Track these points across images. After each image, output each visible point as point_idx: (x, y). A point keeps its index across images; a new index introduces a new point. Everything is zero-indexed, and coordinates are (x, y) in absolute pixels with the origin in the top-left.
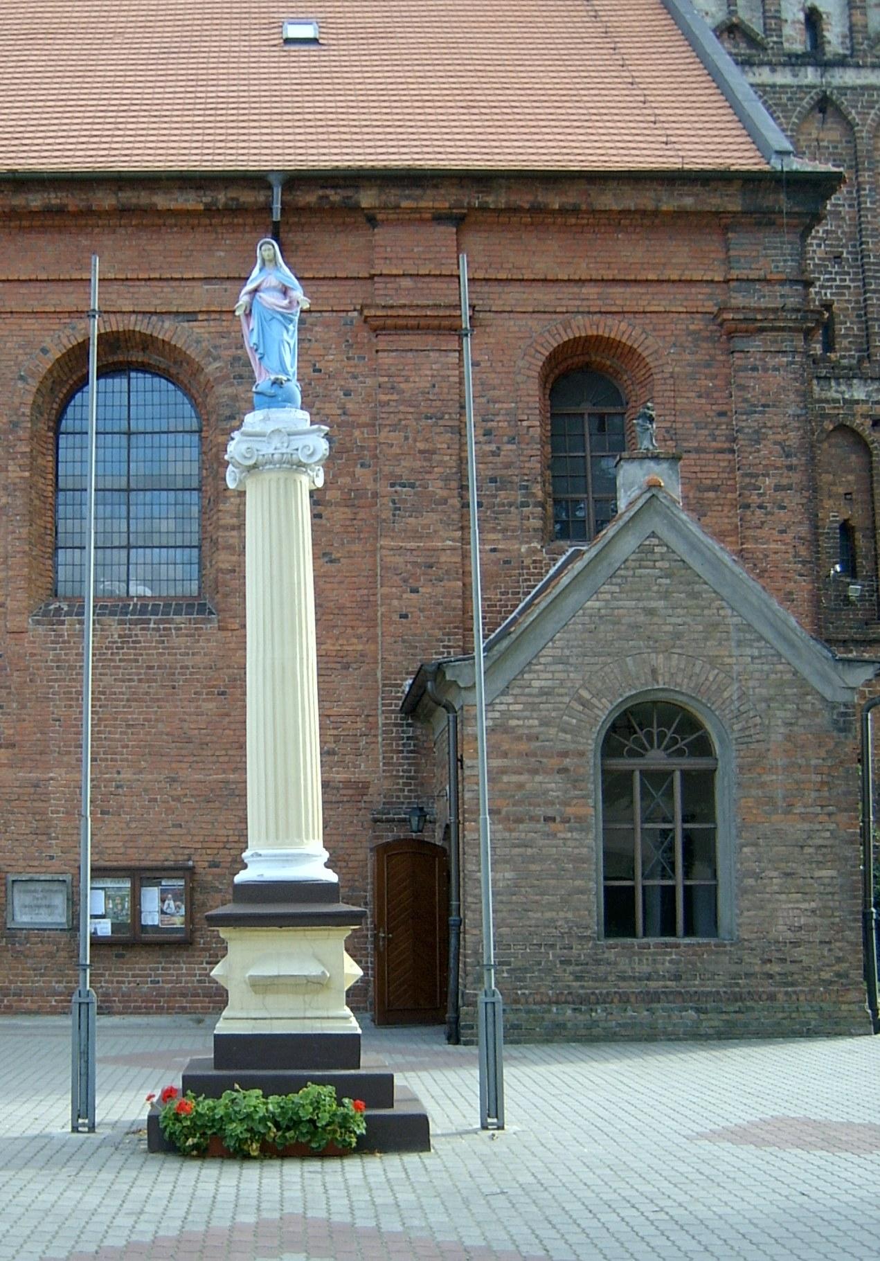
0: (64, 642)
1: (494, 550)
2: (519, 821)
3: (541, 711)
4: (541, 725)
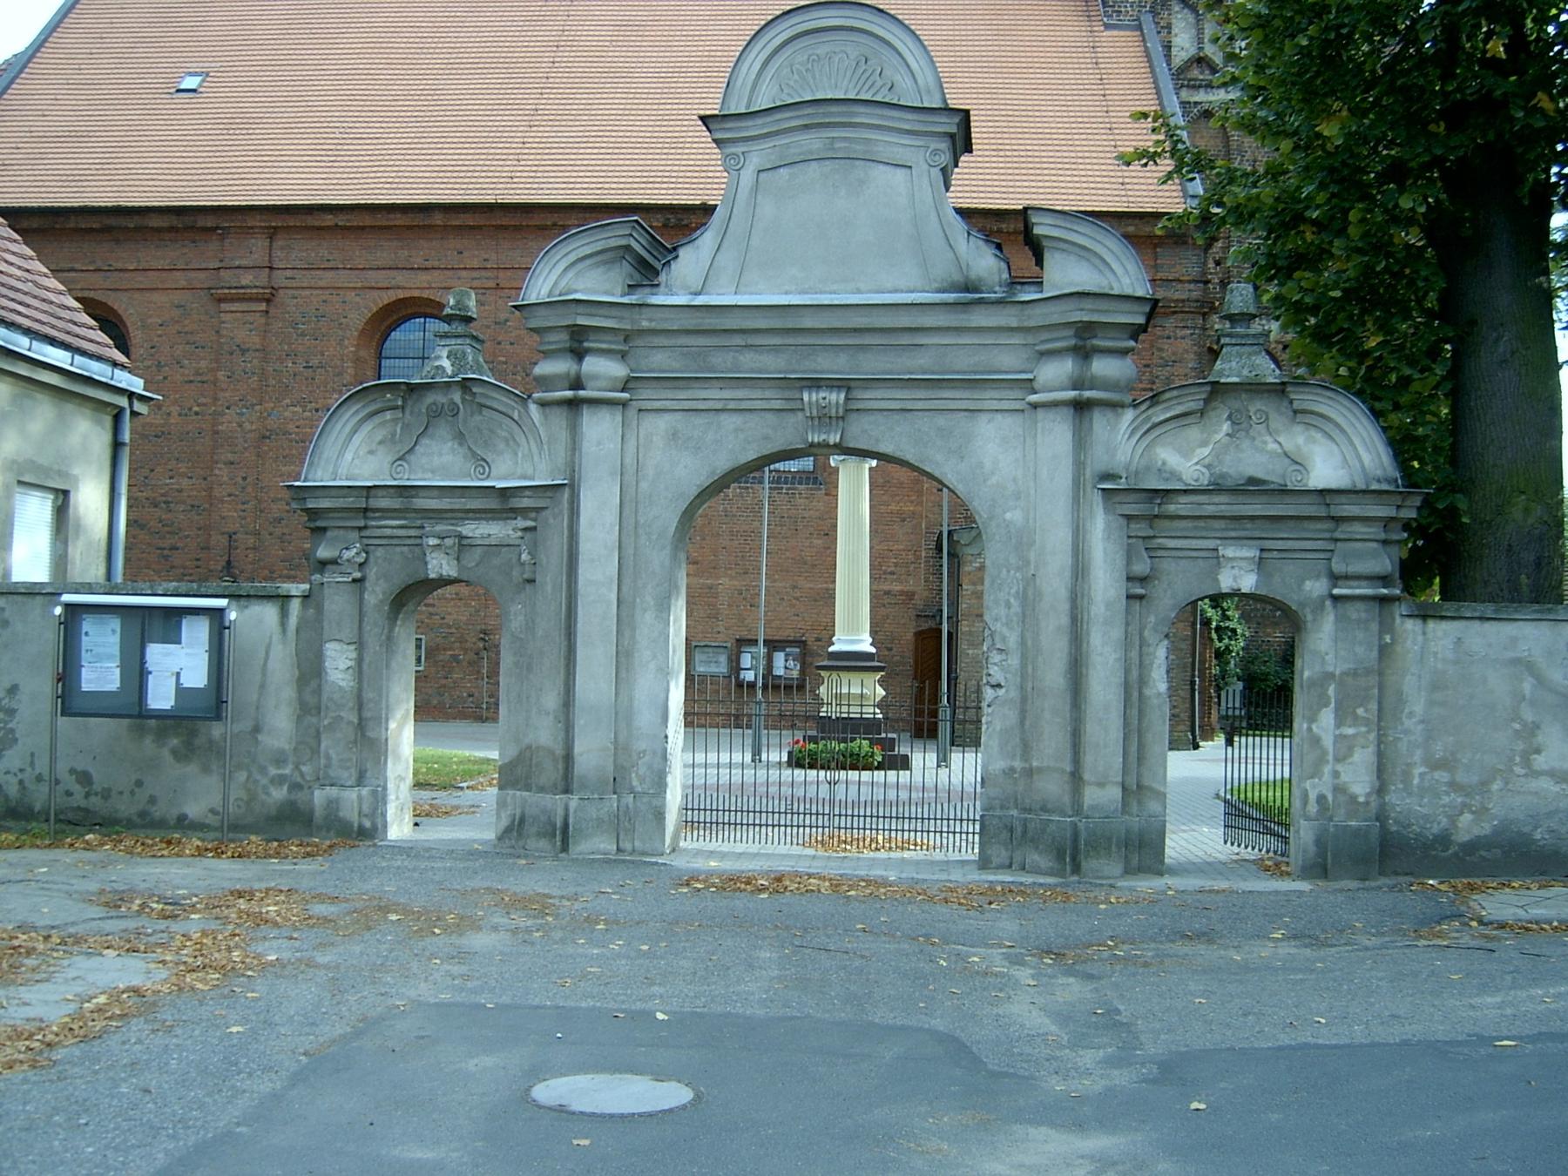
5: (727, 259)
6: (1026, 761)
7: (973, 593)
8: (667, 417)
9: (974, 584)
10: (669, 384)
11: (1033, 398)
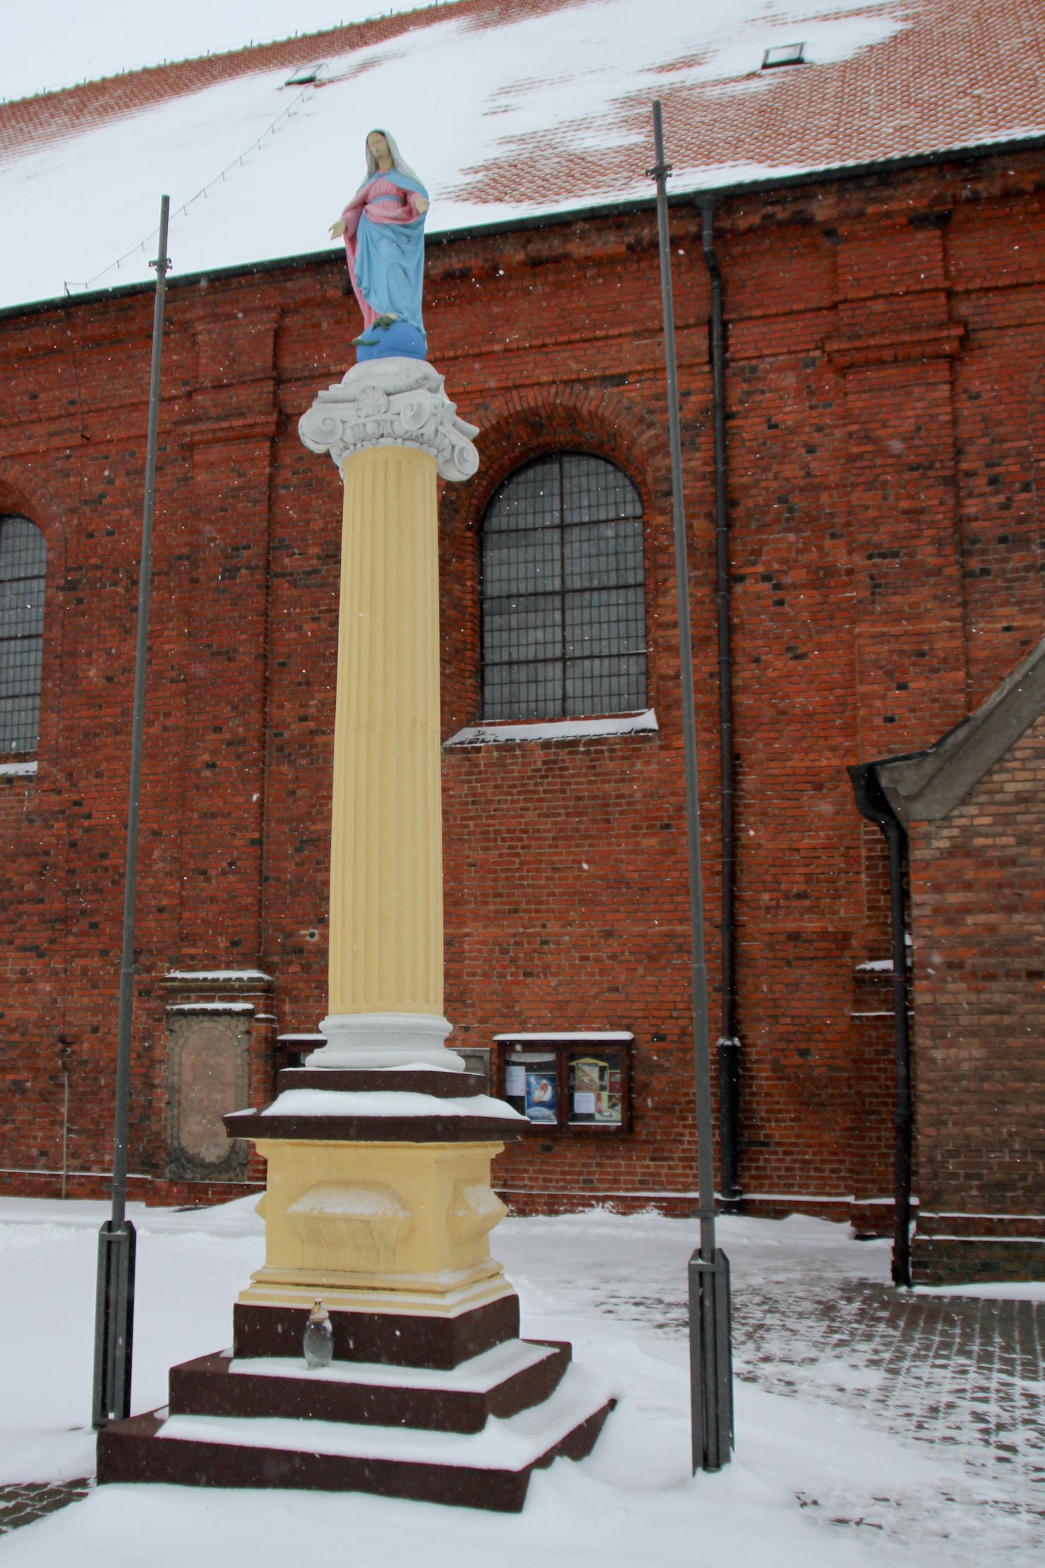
0: (480, 773)
1: (1008, 629)
2: (992, 977)
3: (1017, 824)
4: (1019, 843)
7: (937, 910)
9: (938, 889)
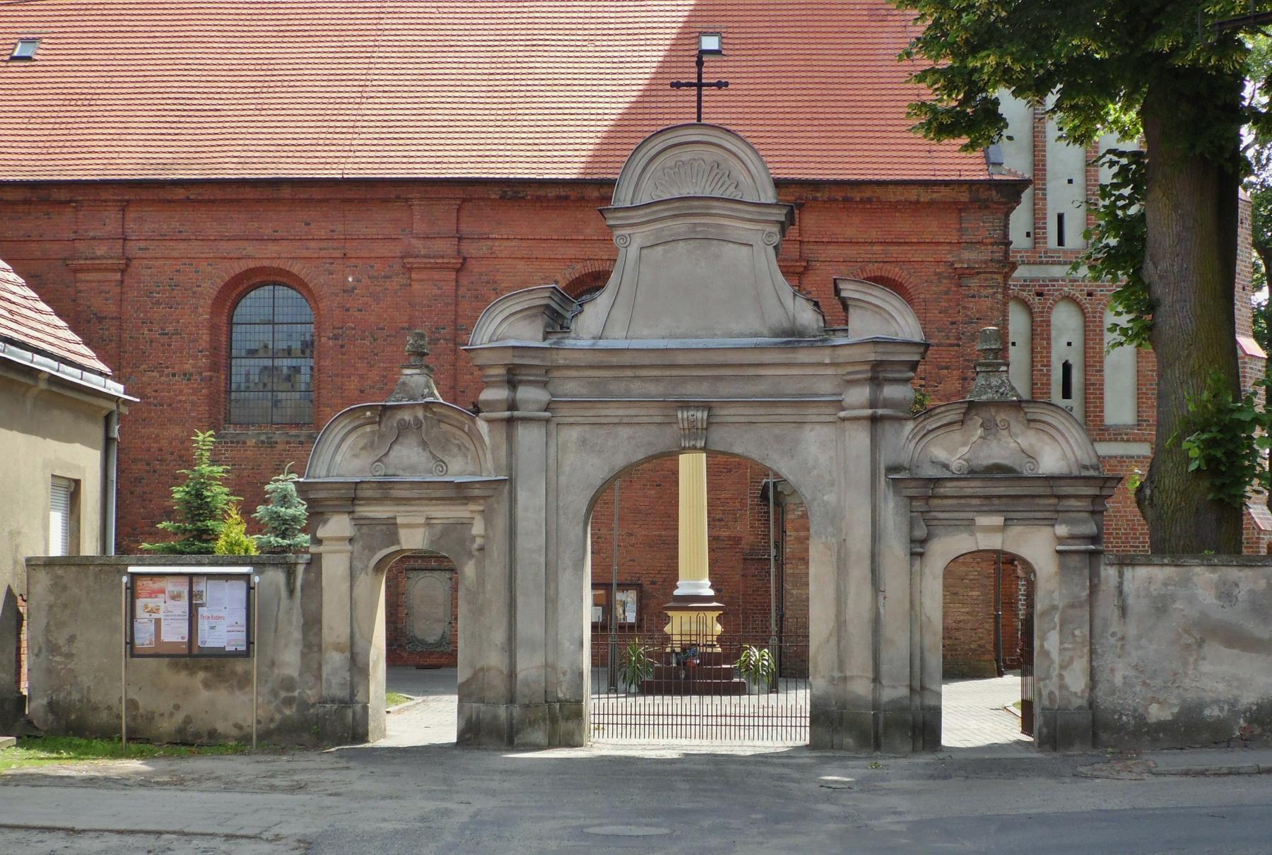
5: (620, 314)
6: (842, 672)
8: (579, 429)
9: (796, 530)
10: (580, 405)
11: (842, 414)
